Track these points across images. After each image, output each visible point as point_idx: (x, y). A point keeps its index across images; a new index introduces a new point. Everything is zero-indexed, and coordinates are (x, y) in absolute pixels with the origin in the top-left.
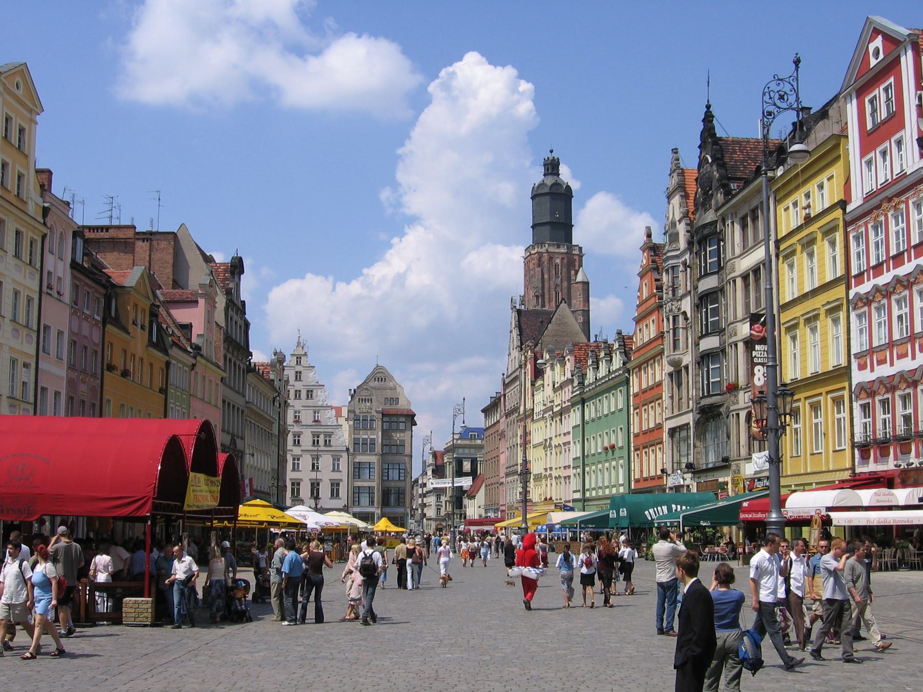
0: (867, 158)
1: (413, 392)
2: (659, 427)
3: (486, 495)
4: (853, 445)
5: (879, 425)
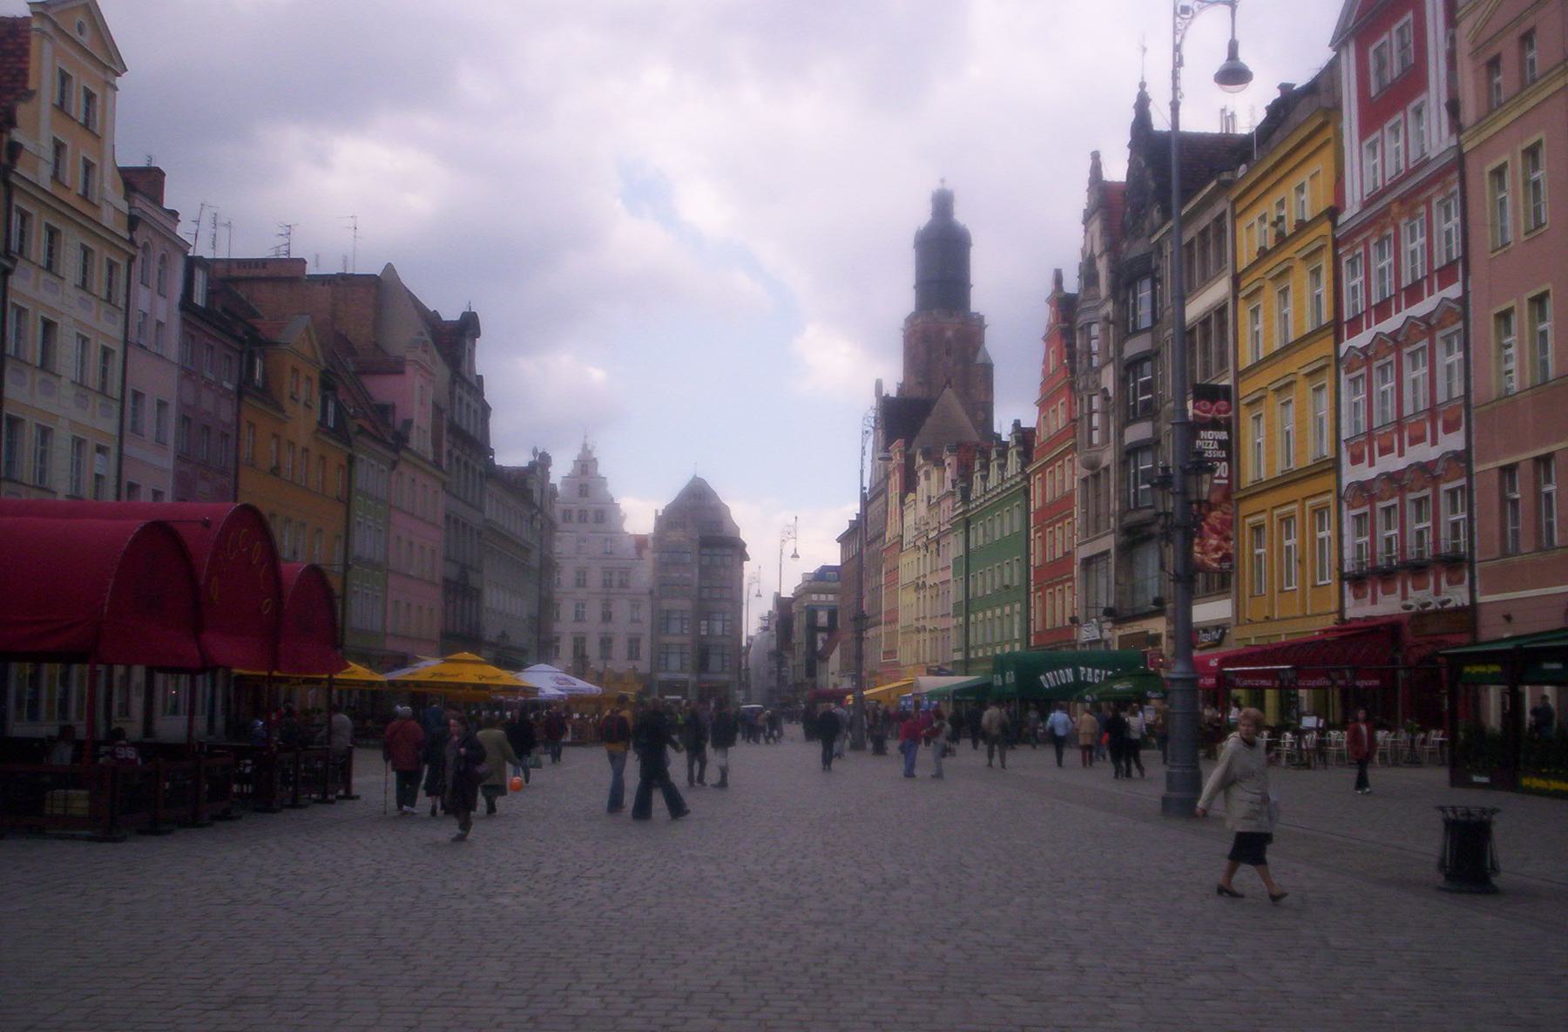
0: (1368, 141)
1: (748, 517)
2: (1068, 555)
3: (842, 657)
4: (1342, 577)
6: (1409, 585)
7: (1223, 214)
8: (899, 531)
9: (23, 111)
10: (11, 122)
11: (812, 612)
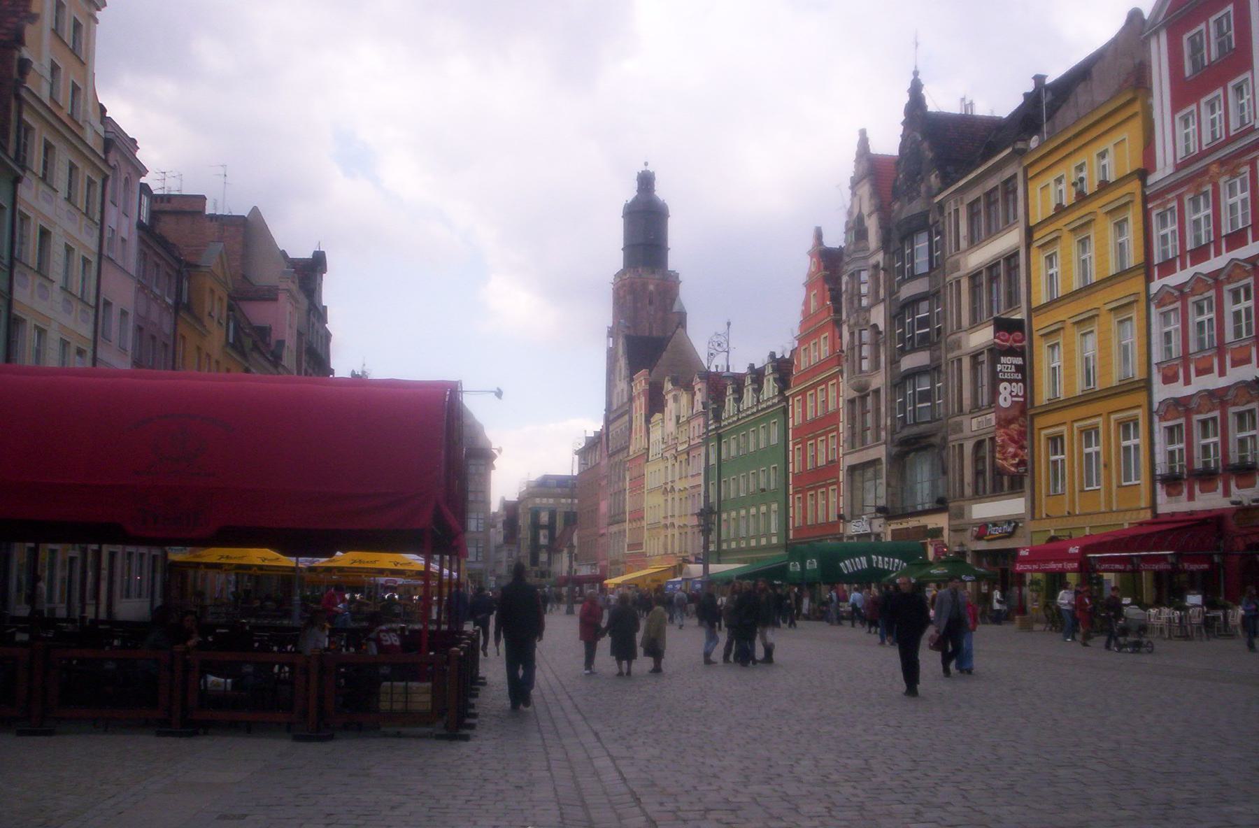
2: (833, 466)
5: (1197, 452)
6: (1197, 488)
7: (1014, 176)
8: (644, 444)
9: (30, 32)
10: (19, 40)
11: (535, 514)
